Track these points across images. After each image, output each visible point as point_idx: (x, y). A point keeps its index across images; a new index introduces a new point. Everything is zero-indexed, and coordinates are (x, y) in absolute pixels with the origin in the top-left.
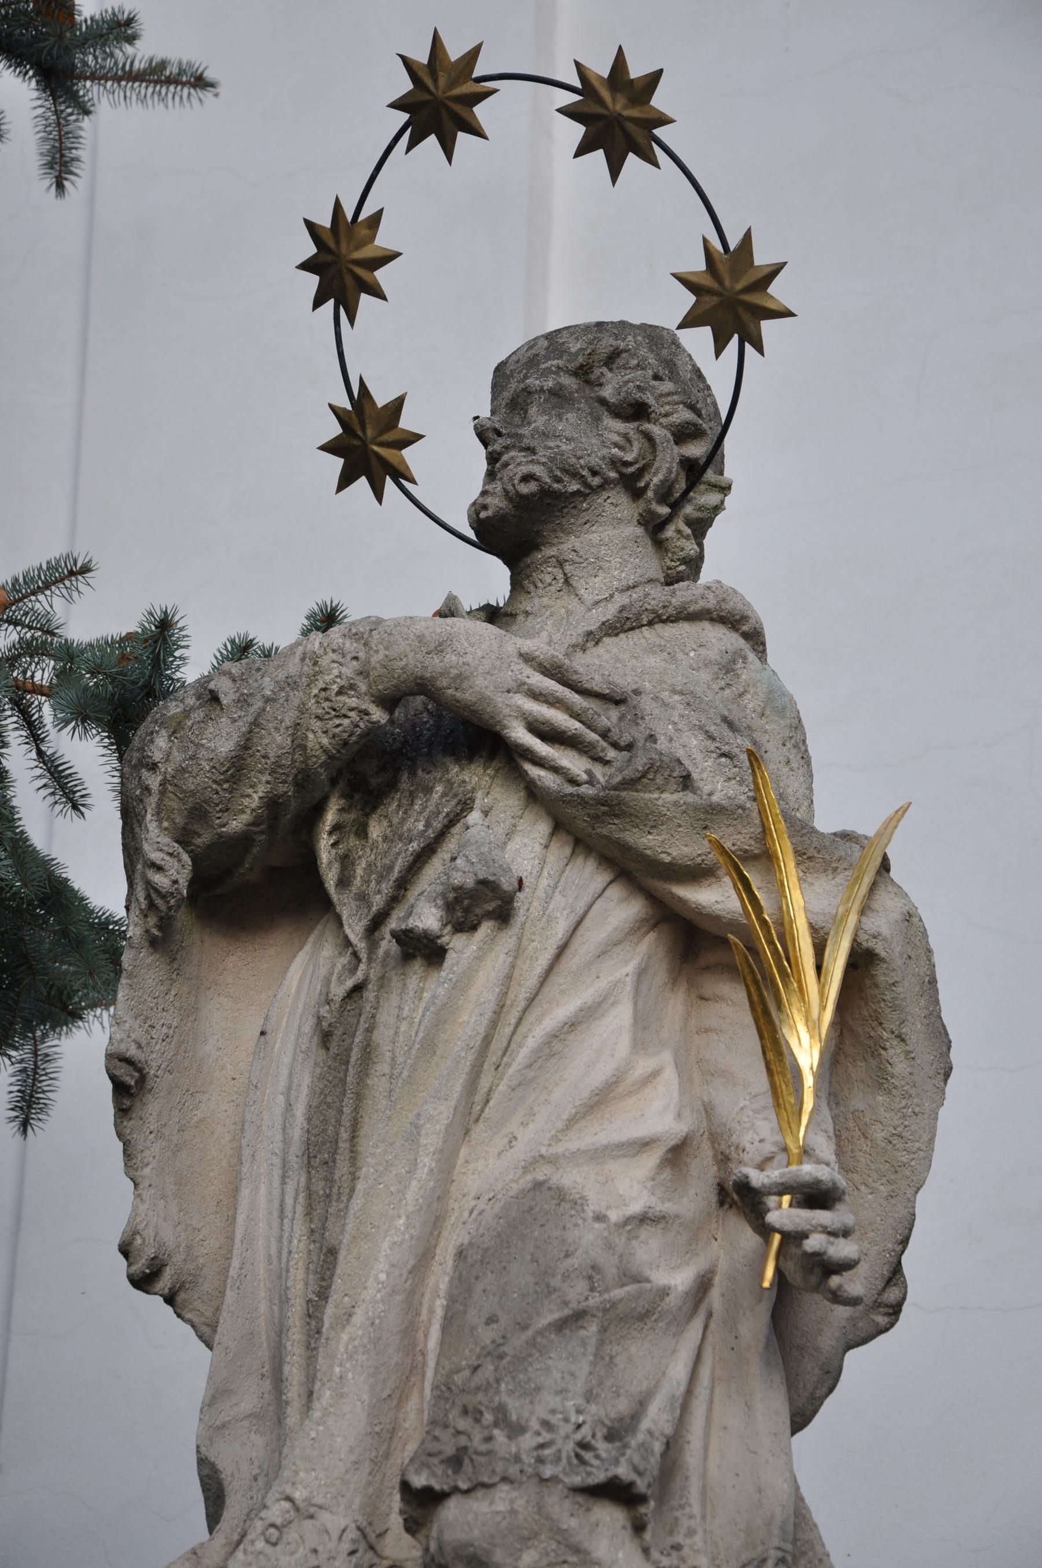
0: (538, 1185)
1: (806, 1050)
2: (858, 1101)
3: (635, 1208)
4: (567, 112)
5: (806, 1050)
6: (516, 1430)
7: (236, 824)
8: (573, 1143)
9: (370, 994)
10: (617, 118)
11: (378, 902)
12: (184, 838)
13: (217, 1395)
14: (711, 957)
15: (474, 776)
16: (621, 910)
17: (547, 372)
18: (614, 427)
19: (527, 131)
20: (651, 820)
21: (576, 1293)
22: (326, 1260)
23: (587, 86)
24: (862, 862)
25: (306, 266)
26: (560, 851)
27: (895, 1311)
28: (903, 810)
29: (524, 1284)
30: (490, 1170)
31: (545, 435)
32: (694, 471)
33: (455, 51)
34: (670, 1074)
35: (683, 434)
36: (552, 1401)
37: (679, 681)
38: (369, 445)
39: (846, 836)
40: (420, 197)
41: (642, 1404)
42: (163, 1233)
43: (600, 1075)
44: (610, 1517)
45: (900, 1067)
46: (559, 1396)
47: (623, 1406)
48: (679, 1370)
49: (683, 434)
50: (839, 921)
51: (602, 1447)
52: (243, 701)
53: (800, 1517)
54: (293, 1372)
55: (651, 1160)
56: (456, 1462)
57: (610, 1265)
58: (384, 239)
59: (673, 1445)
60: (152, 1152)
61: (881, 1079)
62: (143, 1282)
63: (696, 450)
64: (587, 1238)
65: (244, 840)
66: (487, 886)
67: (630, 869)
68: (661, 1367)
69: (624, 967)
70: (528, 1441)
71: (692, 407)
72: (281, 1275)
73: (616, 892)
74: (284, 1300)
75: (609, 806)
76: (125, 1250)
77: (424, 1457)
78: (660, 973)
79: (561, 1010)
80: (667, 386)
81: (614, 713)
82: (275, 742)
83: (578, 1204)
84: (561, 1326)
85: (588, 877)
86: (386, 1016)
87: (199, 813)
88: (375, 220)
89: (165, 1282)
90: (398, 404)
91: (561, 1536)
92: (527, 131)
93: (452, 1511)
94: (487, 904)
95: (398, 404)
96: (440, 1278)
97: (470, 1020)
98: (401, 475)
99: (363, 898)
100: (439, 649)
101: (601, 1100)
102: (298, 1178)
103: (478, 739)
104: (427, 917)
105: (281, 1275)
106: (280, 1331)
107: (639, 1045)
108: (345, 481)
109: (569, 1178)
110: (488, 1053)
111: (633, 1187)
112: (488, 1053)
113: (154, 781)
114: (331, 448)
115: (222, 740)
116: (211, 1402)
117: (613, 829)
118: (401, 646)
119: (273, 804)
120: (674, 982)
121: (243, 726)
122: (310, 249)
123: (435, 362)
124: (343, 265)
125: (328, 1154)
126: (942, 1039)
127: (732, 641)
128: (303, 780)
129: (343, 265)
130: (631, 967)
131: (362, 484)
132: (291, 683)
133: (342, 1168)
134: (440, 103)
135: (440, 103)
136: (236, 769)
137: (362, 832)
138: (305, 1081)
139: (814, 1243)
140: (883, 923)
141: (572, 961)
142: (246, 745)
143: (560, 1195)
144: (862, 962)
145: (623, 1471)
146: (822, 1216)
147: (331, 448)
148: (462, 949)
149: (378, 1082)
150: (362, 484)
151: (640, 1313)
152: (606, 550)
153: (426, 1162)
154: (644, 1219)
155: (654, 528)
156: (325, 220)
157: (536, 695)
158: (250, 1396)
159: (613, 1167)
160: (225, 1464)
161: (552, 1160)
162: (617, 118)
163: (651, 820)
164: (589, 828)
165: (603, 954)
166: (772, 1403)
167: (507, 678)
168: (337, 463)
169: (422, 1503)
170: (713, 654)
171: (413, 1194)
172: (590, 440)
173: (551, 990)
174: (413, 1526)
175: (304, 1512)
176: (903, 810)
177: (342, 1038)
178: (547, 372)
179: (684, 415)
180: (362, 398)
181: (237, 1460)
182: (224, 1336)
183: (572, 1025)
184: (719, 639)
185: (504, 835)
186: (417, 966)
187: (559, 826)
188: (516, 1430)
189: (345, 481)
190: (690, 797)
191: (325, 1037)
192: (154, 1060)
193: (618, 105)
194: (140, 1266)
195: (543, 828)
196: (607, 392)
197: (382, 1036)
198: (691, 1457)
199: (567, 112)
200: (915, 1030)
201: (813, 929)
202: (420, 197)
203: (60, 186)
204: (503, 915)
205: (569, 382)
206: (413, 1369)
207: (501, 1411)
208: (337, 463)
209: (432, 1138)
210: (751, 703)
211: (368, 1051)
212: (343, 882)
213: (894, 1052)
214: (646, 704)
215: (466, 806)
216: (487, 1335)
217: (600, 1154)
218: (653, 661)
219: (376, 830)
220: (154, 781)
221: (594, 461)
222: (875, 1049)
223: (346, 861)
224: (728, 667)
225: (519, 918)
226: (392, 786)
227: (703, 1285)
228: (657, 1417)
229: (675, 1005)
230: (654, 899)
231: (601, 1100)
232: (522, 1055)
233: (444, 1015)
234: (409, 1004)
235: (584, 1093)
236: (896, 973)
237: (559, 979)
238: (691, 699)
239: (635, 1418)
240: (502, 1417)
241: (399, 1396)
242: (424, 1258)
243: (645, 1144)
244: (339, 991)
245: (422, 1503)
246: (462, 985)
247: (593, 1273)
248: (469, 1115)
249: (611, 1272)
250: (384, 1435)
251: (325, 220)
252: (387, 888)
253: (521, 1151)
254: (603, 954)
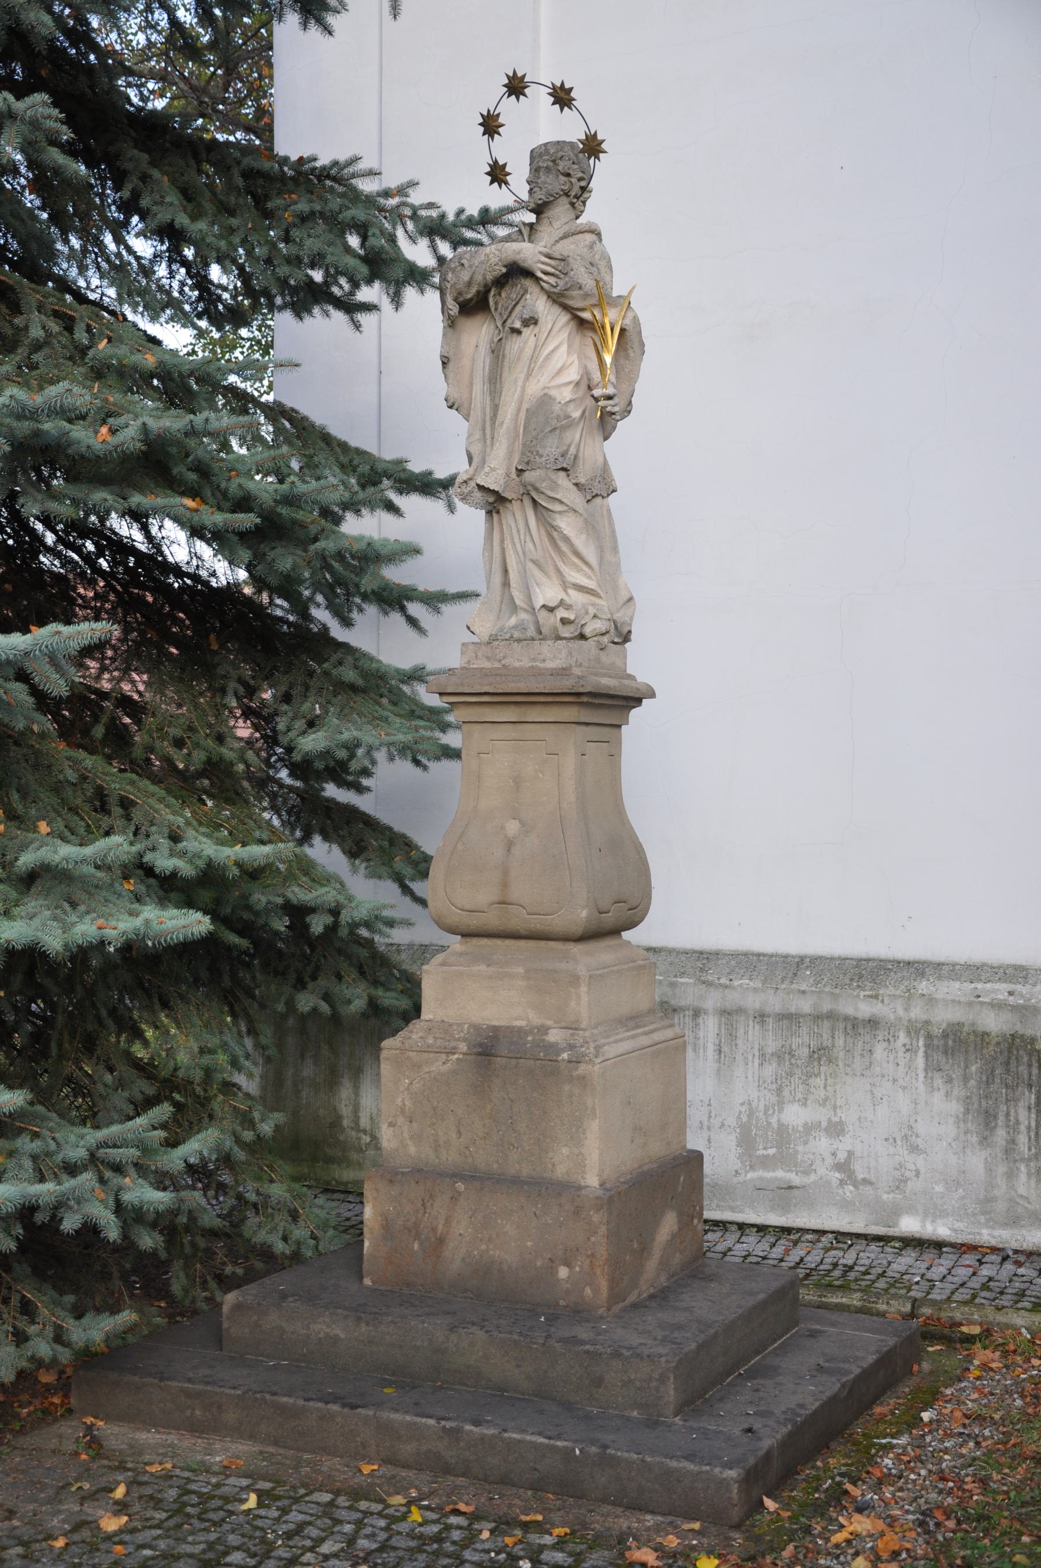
0: (545, 394)
1: (608, 358)
2: (622, 362)
3: (568, 399)
4: (549, 94)
5: (608, 358)
6: (541, 456)
7: (469, 296)
8: (553, 383)
9: (503, 341)
10: (562, 97)
11: (505, 317)
12: (455, 300)
13: (470, 435)
14: (586, 326)
15: (528, 283)
16: (565, 317)
17: (544, 161)
18: (562, 178)
19: (539, 98)
20: (572, 298)
21: (554, 422)
22: (495, 408)
23: (554, 87)
24: (624, 302)
25: (480, 124)
26: (550, 303)
27: (630, 412)
28: (634, 288)
29: (542, 419)
30: (534, 389)
31: (545, 183)
32: (583, 189)
33: (519, 74)
34: (576, 362)
35: (580, 179)
36: (549, 449)
37: (579, 252)
38: (498, 174)
39: (619, 297)
40: (509, 110)
41: (569, 446)
42: (455, 395)
43: (559, 365)
44: (562, 474)
45: (632, 354)
46: (551, 448)
47: (565, 448)
48: (577, 437)
49: (580, 179)
50: (617, 322)
51: (560, 459)
52: (470, 266)
53: (605, 467)
54: (488, 432)
55: (572, 386)
56: (528, 463)
57: (562, 414)
58: (501, 120)
59: (576, 457)
60: (451, 375)
61: (627, 357)
62: (450, 407)
63: (583, 184)
64: (557, 408)
65: (471, 299)
66: (532, 318)
67: (565, 307)
68: (574, 435)
69: (564, 335)
70: (544, 459)
71: (583, 172)
72: (484, 408)
73: (563, 313)
74: (485, 415)
75: (561, 295)
76: (446, 400)
77: (520, 462)
78: (574, 330)
79: (550, 348)
80: (576, 166)
81: (563, 264)
82: (479, 278)
83: (554, 399)
84: (551, 431)
85: (556, 310)
86: (508, 347)
87: (460, 293)
88: (498, 115)
89: (455, 407)
90: (505, 165)
91: (551, 479)
92: (539, 98)
93: (527, 474)
94: (531, 321)
95: (505, 165)
96: (523, 415)
97: (528, 351)
98: (506, 183)
99: (501, 314)
100: (519, 253)
101: (560, 371)
102: (487, 386)
103: (528, 273)
104: (518, 325)
105: (484, 408)
106: (484, 422)
107: (569, 353)
108: (492, 183)
109: (553, 393)
110: (533, 359)
111: (567, 394)
112: (533, 359)
113: (449, 286)
114: (487, 174)
115: (465, 276)
116: (468, 438)
117: (562, 300)
118: (510, 253)
119: (478, 292)
120: (578, 331)
121: (471, 273)
122: (481, 120)
123: (514, 150)
124: (490, 125)
125: (495, 381)
126: (642, 345)
127: (593, 237)
128: (486, 285)
129: (490, 125)
130: (567, 334)
131: (496, 184)
132: (482, 262)
133: (498, 386)
134: (516, 87)
135: (516, 87)
136: (469, 284)
137: (500, 294)
138: (488, 361)
139: (609, 409)
140: (627, 321)
141: (553, 333)
142: (472, 278)
143: (550, 397)
144: (623, 331)
145: (565, 465)
146: (611, 402)
147: (487, 174)
148: (526, 332)
149: (506, 364)
150: (496, 184)
151: (571, 424)
152: (560, 211)
153: (519, 389)
154: (570, 401)
155: (573, 204)
156: (485, 114)
157: (543, 263)
158: (478, 435)
159: (562, 389)
160: (472, 452)
161: (548, 388)
162: (562, 97)
163: (572, 298)
164: (558, 299)
165: (560, 330)
166: (601, 438)
167: (536, 259)
168: (489, 178)
169: (520, 472)
170: (587, 243)
171: (516, 397)
172: (554, 183)
173: (548, 341)
174: (518, 476)
175: (493, 470)
176: (634, 288)
177: (497, 351)
178: (544, 161)
179: (580, 175)
180: (496, 162)
181: (476, 450)
182: (471, 419)
183: (553, 351)
184: (590, 238)
185: (538, 303)
186: (515, 335)
187: (549, 297)
188: (541, 456)
189: (492, 183)
190: (581, 292)
191: (493, 352)
192: (450, 355)
193: (562, 95)
194: (450, 404)
195: (545, 297)
196: (560, 168)
197: (507, 352)
198: (581, 455)
199: (549, 94)
200: (636, 345)
201: (611, 323)
202: (509, 110)
203: (395, 17)
204: (536, 323)
205: (550, 164)
206: (517, 436)
207: (537, 452)
208: (489, 178)
209: (520, 383)
210: (597, 257)
211: (504, 356)
212: (496, 309)
213: (630, 351)
214: (571, 260)
215: (526, 291)
216: (534, 433)
217: (559, 386)
218: (573, 247)
219: (503, 294)
220: (449, 286)
221: (557, 191)
222: (626, 350)
223: (496, 303)
224: (591, 247)
225: (540, 322)
226: (507, 282)
227: (584, 412)
228: (572, 451)
229: (577, 339)
230: (572, 313)
231: (560, 371)
232: (541, 359)
233: (521, 350)
234: (514, 345)
235: (555, 371)
236: (631, 333)
237: (550, 338)
238: (582, 258)
239: (568, 450)
240: (538, 453)
241: (513, 443)
242: (519, 410)
243: (570, 383)
244: (496, 340)
245: (520, 472)
246: (526, 343)
247: (558, 417)
248: (529, 375)
249: (562, 416)
250: (510, 453)
251: (485, 114)
252: (507, 313)
253: (541, 385)
254: (560, 330)
